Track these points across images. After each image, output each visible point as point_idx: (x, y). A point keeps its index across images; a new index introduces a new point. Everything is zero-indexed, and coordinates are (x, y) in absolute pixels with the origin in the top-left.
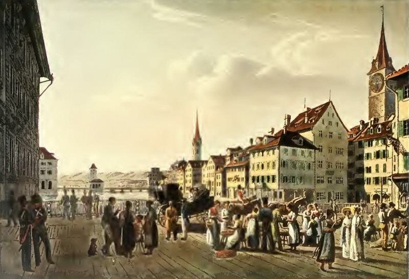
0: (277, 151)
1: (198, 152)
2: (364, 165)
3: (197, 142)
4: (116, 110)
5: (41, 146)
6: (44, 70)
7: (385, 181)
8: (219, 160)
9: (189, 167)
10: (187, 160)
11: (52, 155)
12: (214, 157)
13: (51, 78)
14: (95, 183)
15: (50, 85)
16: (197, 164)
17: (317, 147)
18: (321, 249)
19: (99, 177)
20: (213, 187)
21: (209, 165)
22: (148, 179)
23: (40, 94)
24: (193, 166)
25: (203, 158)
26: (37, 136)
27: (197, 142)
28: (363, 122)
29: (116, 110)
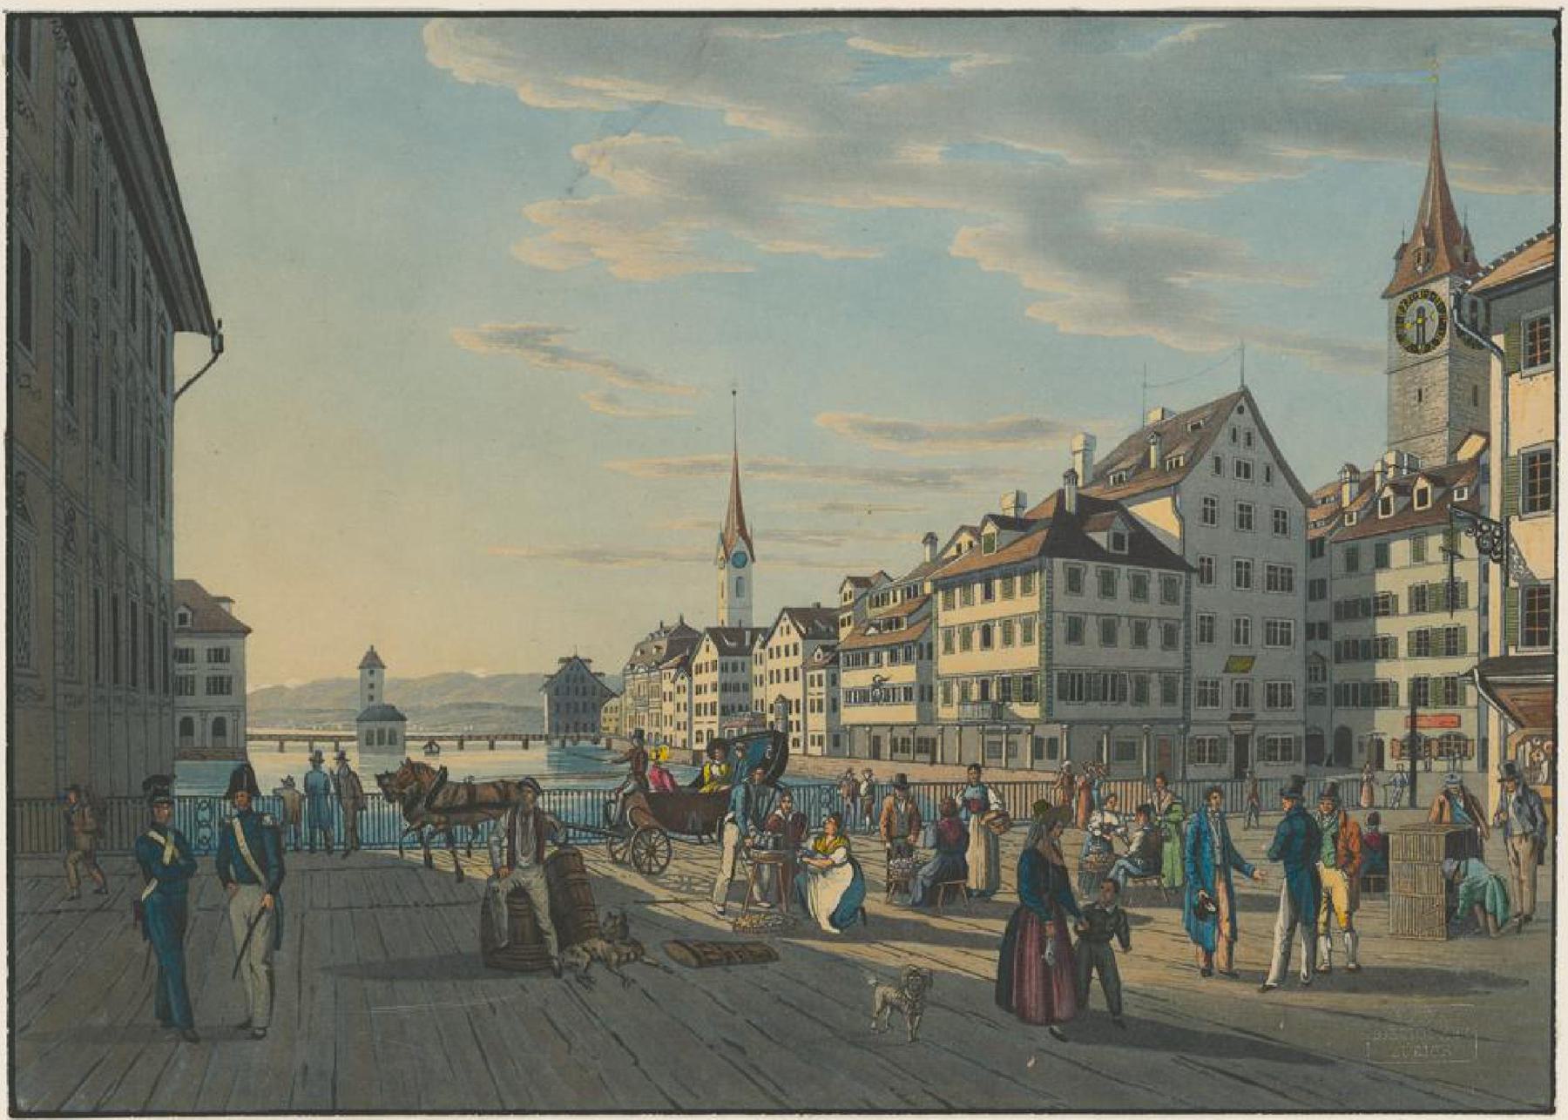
0: (1037, 580)
1: (740, 587)
2: (919, 709)
3: (738, 548)
4: (393, 538)
5: (181, 573)
6: (188, 304)
7: (1451, 690)
8: (815, 623)
9: (707, 654)
10: (698, 623)
11: (224, 606)
12: (796, 614)
13: (210, 328)
14: (375, 726)
15: (209, 365)
16: (736, 642)
17: (1195, 564)
18: (1307, 986)
19: (389, 699)
20: (800, 717)
21: (777, 640)
22: (544, 701)
23: (178, 386)
24: (723, 651)
25: (761, 617)
26: (166, 535)
27: (738, 548)
28: (1353, 470)
29: (393, 538)
